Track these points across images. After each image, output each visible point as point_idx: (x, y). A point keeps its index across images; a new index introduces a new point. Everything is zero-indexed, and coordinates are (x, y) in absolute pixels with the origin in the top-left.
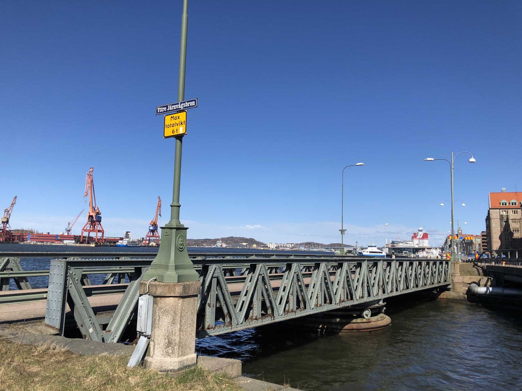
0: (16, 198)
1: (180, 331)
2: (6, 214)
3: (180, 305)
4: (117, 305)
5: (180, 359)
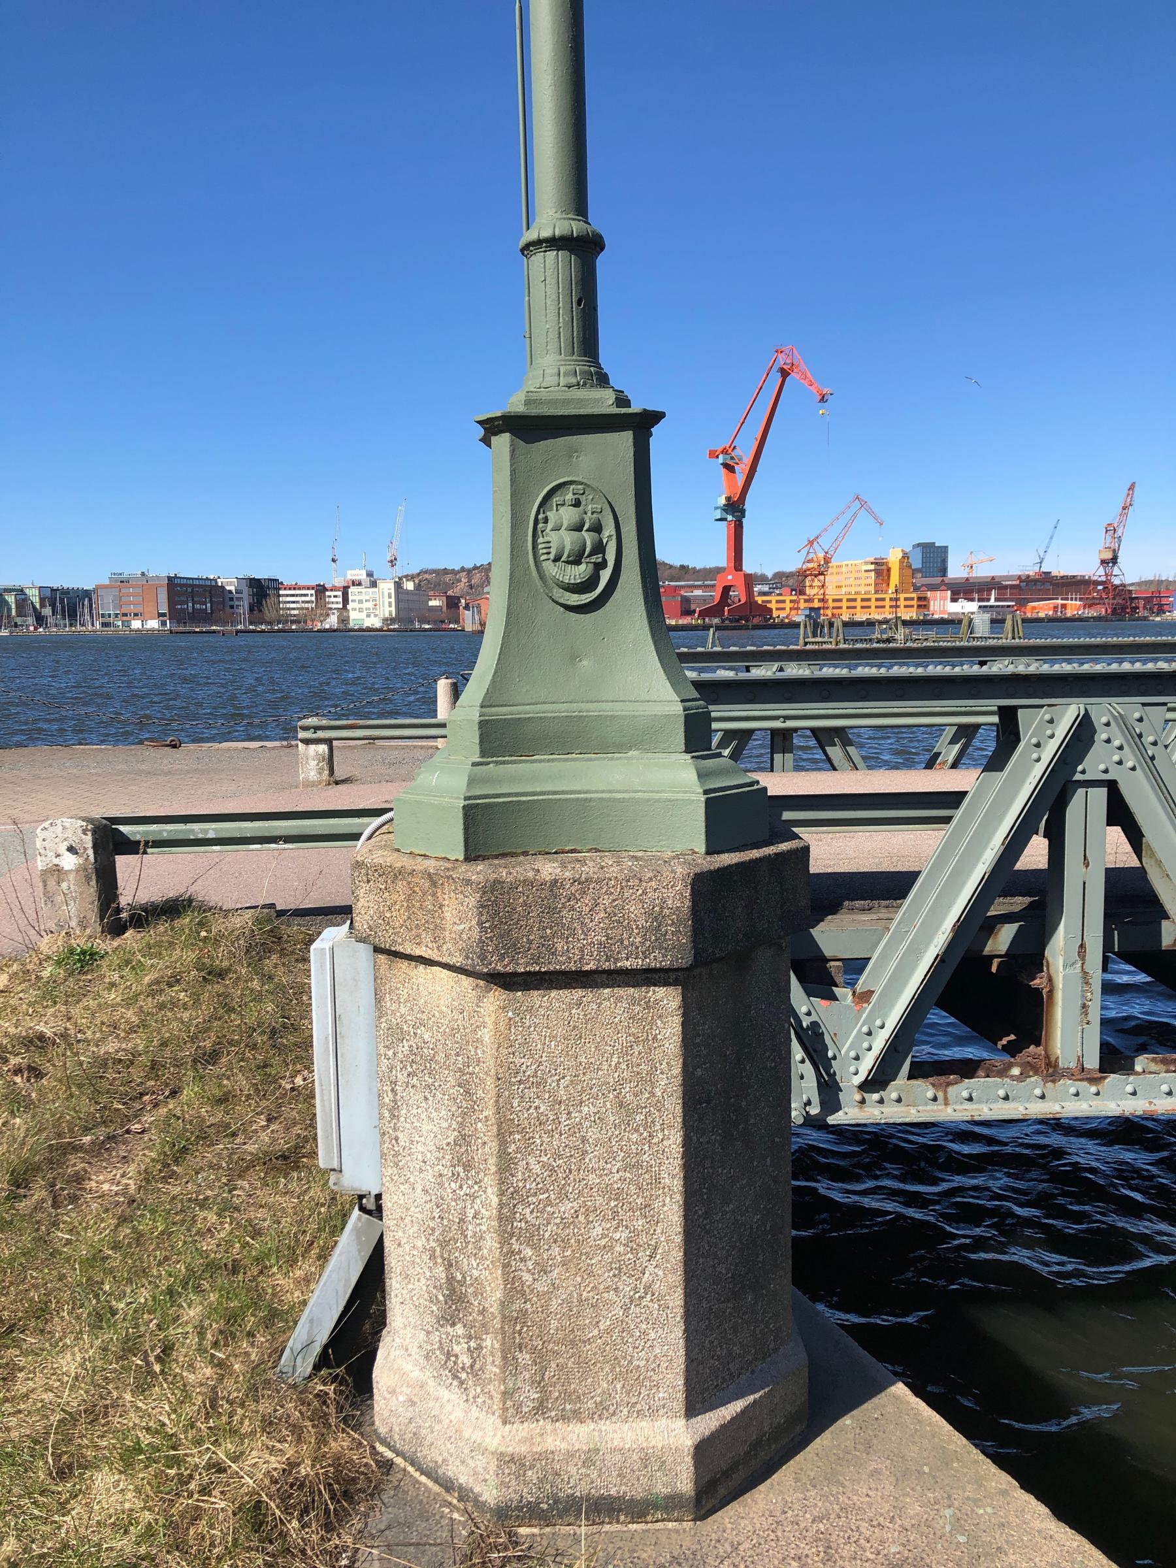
0: (1132, 487)
1: (505, 1237)
2: (1109, 539)
3: (486, 1034)
4: (912, 876)
5: (517, 1437)
